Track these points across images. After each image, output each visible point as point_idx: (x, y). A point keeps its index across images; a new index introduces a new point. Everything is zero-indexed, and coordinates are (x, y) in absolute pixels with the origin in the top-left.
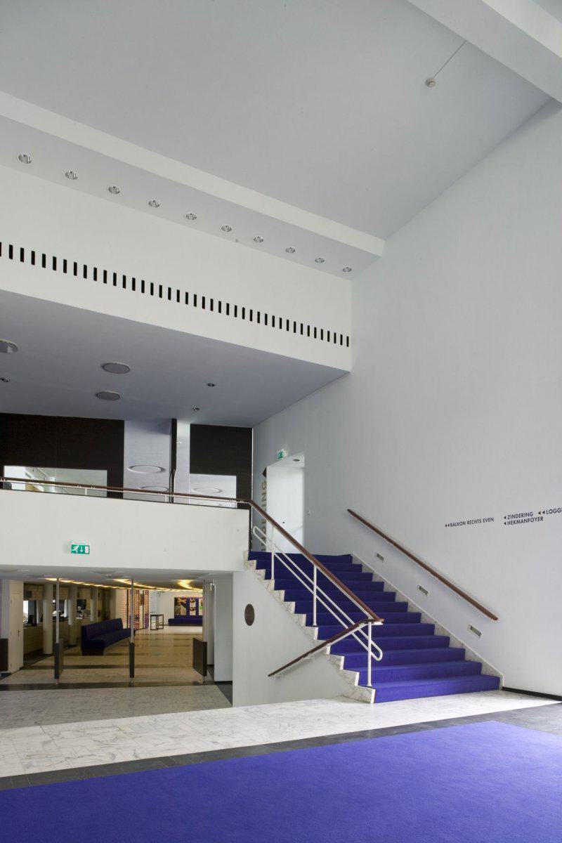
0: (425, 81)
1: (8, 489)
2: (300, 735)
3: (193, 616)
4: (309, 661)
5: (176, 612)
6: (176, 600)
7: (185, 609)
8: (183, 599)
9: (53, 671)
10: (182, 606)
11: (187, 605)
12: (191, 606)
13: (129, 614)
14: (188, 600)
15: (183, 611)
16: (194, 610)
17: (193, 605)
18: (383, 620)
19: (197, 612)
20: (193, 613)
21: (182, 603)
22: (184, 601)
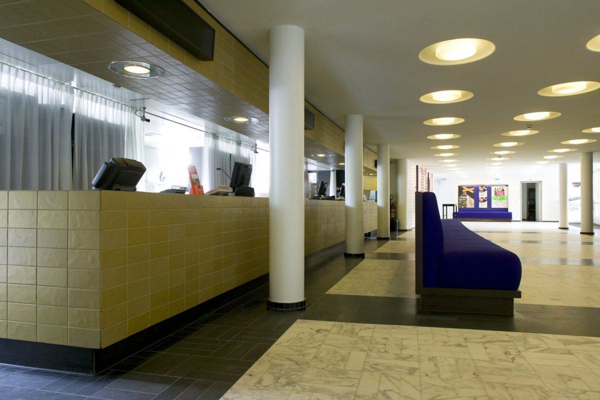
3: (483, 209)
6: (461, 189)
7: (473, 200)
8: (469, 187)
9: (448, 207)
10: (468, 197)
11: (475, 195)
12: (480, 197)
14: (477, 189)
15: (470, 203)
16: (484, 201)
17: (483, 195)
18: (423, 57)
20: (483, 205)
21: (468, 193)
22: (471, 190)
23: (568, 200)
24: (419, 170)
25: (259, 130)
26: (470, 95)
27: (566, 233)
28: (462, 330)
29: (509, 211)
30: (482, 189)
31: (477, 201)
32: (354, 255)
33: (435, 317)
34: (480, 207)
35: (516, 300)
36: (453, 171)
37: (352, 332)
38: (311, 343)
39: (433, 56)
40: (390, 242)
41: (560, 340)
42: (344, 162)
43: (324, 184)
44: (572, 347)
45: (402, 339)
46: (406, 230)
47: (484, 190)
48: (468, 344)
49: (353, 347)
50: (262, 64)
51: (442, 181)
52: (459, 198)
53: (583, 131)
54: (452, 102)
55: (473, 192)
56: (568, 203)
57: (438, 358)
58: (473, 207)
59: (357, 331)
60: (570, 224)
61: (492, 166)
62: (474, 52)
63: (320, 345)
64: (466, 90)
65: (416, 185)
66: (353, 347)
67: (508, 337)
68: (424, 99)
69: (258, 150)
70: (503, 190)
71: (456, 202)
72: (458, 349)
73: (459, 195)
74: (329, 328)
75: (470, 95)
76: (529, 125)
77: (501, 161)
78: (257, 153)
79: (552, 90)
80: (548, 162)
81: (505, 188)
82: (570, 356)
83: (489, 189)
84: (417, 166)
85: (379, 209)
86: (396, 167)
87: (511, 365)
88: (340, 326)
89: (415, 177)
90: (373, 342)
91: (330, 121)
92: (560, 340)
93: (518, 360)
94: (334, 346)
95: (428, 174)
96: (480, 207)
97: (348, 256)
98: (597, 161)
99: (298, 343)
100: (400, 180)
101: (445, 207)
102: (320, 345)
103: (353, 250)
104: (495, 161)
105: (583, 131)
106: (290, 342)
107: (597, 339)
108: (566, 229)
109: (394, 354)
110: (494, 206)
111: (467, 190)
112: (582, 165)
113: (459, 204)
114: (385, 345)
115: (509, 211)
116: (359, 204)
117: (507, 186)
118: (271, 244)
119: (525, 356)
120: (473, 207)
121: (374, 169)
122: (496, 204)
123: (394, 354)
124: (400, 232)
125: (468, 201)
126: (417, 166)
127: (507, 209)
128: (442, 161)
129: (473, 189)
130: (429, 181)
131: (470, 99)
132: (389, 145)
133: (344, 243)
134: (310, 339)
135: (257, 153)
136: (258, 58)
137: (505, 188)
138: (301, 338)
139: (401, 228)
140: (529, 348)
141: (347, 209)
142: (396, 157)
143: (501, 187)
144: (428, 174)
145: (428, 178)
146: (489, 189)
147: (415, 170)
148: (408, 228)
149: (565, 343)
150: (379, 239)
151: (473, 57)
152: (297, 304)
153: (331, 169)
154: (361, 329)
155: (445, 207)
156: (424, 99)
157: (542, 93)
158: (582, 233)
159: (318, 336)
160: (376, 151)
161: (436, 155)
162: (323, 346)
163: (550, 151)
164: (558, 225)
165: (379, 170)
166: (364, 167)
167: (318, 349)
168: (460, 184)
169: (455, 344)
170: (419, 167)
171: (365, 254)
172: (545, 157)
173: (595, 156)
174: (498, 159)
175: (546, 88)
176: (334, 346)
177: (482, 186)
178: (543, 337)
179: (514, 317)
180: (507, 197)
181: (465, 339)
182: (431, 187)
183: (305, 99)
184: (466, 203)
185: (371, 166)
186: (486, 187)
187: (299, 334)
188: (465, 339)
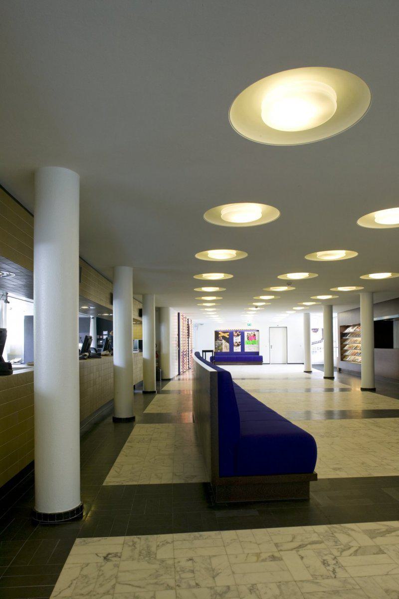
0: (331, 409)
1: (33, 374)
2: (279, 531)
3: (237, 353)
4: (54, 525)
5: (218, 347)
6: (217, 333)
7: (228, 344)
8: (224, 332)
9: (207, 353)
10: (224, 341)
11: (230, 340)
12: (234, 341)
13: (181, 348)
14: (231, 334)
15: (225, 347)
16: (238, 345)
17: (237, 339)
18: (208, 218)
19: (243, 348)
20: (237, 349)
21: (224, 338)
22: (226, 335)
23: (311, 343)
24: (181, 317)
25: (14, 284)
26: (244, 255)
27: (309, 378)
28: (269, 529)
29: (260, 355)
30: (236, 334)
31: (232, 346)
32: (124, 419)
33: (234, 513)
34: (235, 351)
35: (312, 483)
36: (207, 311)
37: (149, 555)
38: (101, 585)
39: (218, 216)
40: (157, 396)
41: (366, 532)
42: (112, 313)
43: (88, 339)
44: (380, 541)
45: (210, 557)
46: (169, 380)
47: (238, 335)
48: (282, 553)
49: (156, 583)
50: (11, 199)
51: (200, 326)
52: (215, 343)
53: (331, 289)
54: (230, 260)
55: (228, 337)
56: (312, 347)
57: (259, 586)
58: (228, 351)
59: (153, 549)
60: (314, 366)
61: (248, 314)
62: (259, 216)
63: (114, 587)
64: (241, 250)
65: (177, 333)
66: (156, 583)
67: (316, 535)
68: (199, 256)
69: (9, 299)
70: (255, 335)
71: (213, 348)
72: (273, 563)
73: (216, 340)
74: (118, 549)
75: (244, 255)
76: (289, 283)
77: (258, 311)
78: (9, 302)
79: (317, 255)
80: (295, 312)
81: (256, 333)
82: (384, 555)
83: (242, 334)
84: (179, 314)
85: (145, 361)
86: (160, 316)
87: (335, 583)
88: (131, 544)
89: (177, 324)
90: (178, 569)
91: (106, 280)
92: (366, 532)
93: (340, 574)
94: (133, 586)
95: (188, 320)
96: (235, 351)
97: (117, 421)
98: (335, 312)
99: (84, 587)
100: (163, 329)
101: (204, 353)
102: (114, 587)
103: (123, 413)
104: (251, 311)
105: (331, 289)
106: (73, 587)
107: (395, 524)
108: (310, 372)
109: (208, 588)
110: (247, 350)
111: (223, 334)
112: (325, 316)
113: (216, 348)
114: (193, 572)
115: (260, 355)
116: (129, 363)
117: (258, 331)
118: (36, 438)
119: (344, 564)
120: (228, 351)
121: (139, 318)
122: (249, 348)
123: (208, 588)
124: (164, 382)
125: (223, 345)
126: (179, 314)
127: (258, 353)
128: (200, 305)
129: (228, 334)
130: (188, 327)
131: (246, 258)
132: (154, 295)
133: (112, 403)
134: (99, 576)
135: (9, 302)
136: (26, 209)
137: (256, 333)
138: (86, 576)
139: (165, 378)
140: (344, 550)
141: (115, 368)
142: (159, 306)
143: (253, 332)
144: (188, 320)
145: (188, 325)
146: (242, 334)
147: (177, 318)
148: (171, 378)
149: (372, 534)
150: (145, 393)
151: (343, 258)
152: (72, 512)
153: (91, 317)
154: (158, 546)
155: (204, 353)
156: (199, 256)
157: (308, 257)
158: (325, 378)
159: (108, 567)
160: (141, 300)
161: (198, 305)
162: (119, 588)
163: (299, 304)
164: (302, 368)
165: (145, 320)
166: (134, 319)
167: (113, 595)
168: (217, 329)
169: (269, 556)
170: (181, 314)
171: (136, 417)
172: (294, 308)
173: (334, 308)
174: (255, 309)
175: (313, 254)
176: (133, 586)
177: (236, 331)
178: (349, 529)
179: (311, 501)
180: (258, 341)
181: (276, 545)
182: (190, 330)
183: (80, 257)
184: (222, 347)
185: (135, 315)
186: (239, 332)
187: (82, 569)
188: (276, 545)
